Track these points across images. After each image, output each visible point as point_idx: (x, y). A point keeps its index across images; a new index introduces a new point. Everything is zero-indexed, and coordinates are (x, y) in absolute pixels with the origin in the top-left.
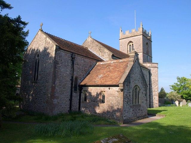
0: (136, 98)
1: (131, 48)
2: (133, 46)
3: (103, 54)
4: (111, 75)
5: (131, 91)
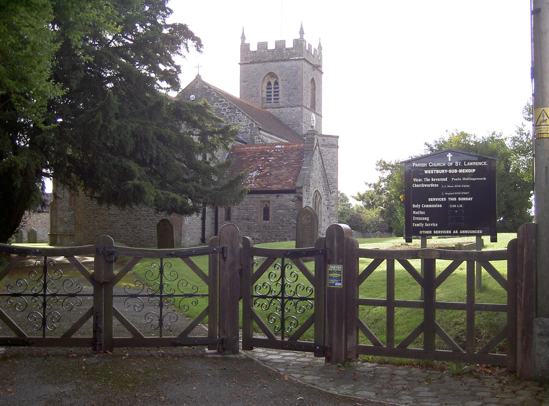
1: (273, 90)
2: (276, 86)
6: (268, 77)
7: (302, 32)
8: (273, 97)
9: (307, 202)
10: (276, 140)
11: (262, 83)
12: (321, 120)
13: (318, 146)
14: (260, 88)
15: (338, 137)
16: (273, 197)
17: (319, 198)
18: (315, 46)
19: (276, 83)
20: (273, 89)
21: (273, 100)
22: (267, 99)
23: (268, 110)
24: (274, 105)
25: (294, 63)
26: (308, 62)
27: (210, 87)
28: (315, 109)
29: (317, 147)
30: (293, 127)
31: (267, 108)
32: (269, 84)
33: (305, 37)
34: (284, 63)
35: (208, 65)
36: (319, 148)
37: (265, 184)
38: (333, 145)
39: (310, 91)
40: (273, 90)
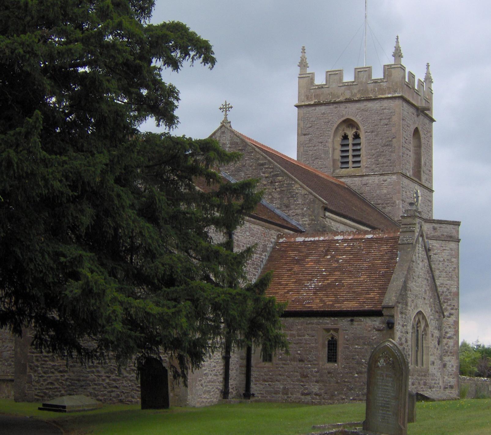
0: (417, 351)
1: (350, 148)
2: (357, 141)
3: (285, 201)
4: (348, 281)
5: (409, 328)
6: (344, 126)
7: (398, 54)
8: (351, 159)
9: (402, 335)
10: (350, 226)
11: (334, 136)
12: (432, 197)
13: (422, 236)
14: (330, 145)
15: (457, 224)
16: (343, 323)
17: (423, 325)
18: (420, 76)
19: (357, 136)
20: (350, 146)
21: (350, 163)
22: (342, 163)
23: (342, 180)
24: (351, 171)
25: (385, 103)
26: (408, 102)
27: (243, 141)
28: (420, 179)
29: (420, 239)
30: (384, 208)
31: (342, 177)
32: (345, 137)
33: (404, 62)
34: (370, 105)
35: (234, 97)
36: (423, 239)
37: (331, 301)
38: (451, 237)
39: (412, 149)
40: (350, 148)
